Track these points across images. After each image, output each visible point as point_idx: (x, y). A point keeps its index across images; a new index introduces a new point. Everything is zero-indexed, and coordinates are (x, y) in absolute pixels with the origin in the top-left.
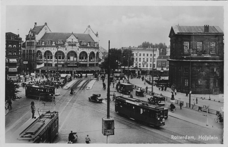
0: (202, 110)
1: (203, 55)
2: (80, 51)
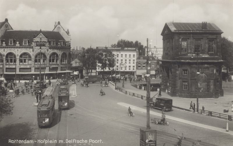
0: (212, 114)
1: (201, 55)
2: (6, 52)
